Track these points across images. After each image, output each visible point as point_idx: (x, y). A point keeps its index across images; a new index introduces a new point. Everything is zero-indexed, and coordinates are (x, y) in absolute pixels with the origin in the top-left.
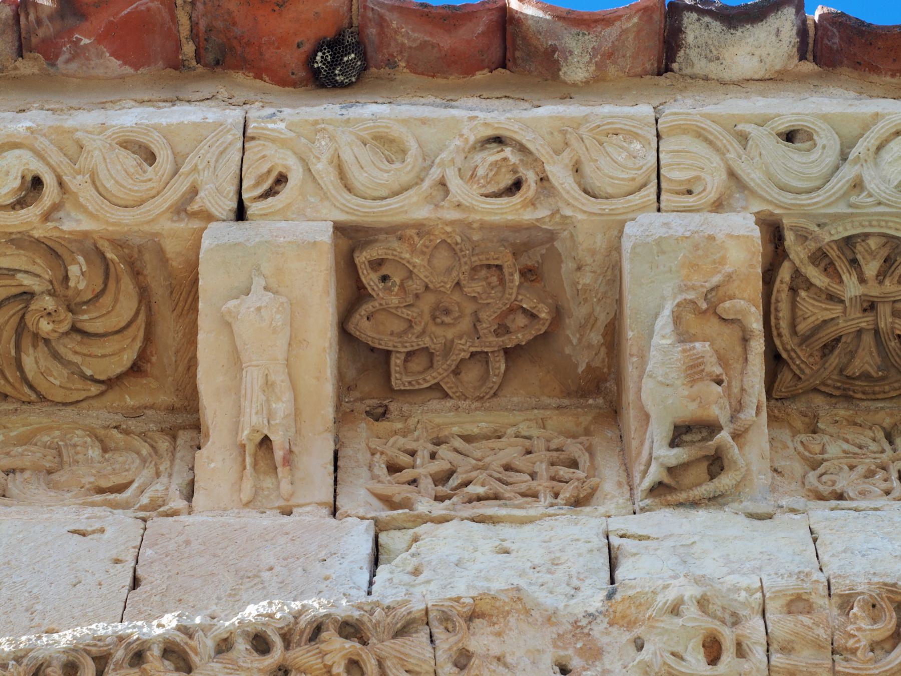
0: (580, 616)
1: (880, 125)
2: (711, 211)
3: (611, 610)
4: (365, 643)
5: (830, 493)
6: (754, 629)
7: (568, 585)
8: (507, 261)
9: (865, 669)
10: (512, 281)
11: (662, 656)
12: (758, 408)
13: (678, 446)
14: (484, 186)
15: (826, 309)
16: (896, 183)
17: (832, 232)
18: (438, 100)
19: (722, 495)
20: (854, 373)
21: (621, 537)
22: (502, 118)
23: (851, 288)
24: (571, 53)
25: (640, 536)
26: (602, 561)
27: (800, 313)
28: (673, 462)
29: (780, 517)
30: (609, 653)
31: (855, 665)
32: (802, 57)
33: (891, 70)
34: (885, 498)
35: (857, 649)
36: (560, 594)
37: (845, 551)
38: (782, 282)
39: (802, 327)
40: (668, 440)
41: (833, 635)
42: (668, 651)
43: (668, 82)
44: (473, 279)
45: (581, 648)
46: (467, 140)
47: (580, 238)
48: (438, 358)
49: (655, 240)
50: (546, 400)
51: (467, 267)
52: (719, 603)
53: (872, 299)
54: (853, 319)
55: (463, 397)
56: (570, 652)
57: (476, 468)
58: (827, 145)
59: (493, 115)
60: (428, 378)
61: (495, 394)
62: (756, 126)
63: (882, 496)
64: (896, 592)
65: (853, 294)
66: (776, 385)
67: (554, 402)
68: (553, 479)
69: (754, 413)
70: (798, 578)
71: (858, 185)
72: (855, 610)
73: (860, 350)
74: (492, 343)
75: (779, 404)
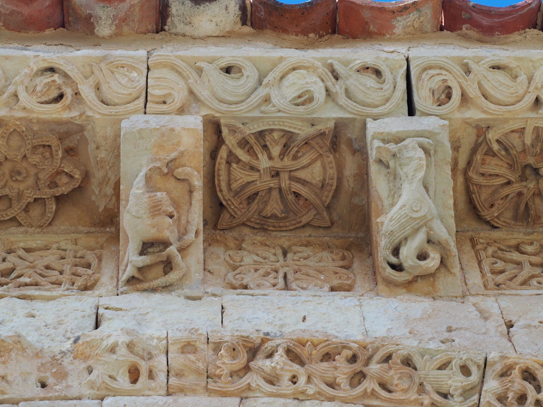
0: (57, 353)
1: (283, 64)
2: (176, 114)
3: (75, 350)
5: (240, 285)
6: (160, 362)
7: (64, 336)
8: (54, 142)
9: (226, 388)
10: (57, 155)
11: (102, 378)
12: (197, 233)
13: (145, 255)
14: (40, 97)
15: (249, 175)
16: (290, 99)
17: (251, 128)
18: (20, 46)
19: (171, 285)
20: (267, 215)
21: (106, 309)
22: (54, 57)
23: (264, 163)
24: (100, 18)
25: (116, 308)
26: (90, 322)
27: (232, 177)
28: (141, 265)
30: (71, 375)
31: (219, 385)
32: (244, 23)
33: (295, 32)
34: (272, 288)
35: (221, 375)
36: (58, 341)
37: (238, 319)
38: (221, 158)
39: (234, 186)
40: (139, 251)
41: (208, 367)
42: (107, 375)
43: (161, 37)
44: (34, 154)
45: (55, 372)
46: (32, 69)
47: (98, 129)
48: (15, 202)
49: (137, 131)
50: (81, 228)
51: (30, 146)
52: (141, 346)
53: (277, 169)
54: (265, 182)
55: (30, 226)
56: (48, 374)
57: (27, 267)
58: (250, 75)
59: (49, 54)
60: (9, 213)
61: (50, 224)
62: (207, 64)
63: (270, 287)
64: (248, 341)
65: (265, 166)
66: (220, 221)
67: (86, 229)
68: (74, 274)
69: (193, 235)
70: (190, 332)
71: (267, 100)
72: (222, 351)
73: (271, 200)
74: (47, 193)
75: (222, 232)
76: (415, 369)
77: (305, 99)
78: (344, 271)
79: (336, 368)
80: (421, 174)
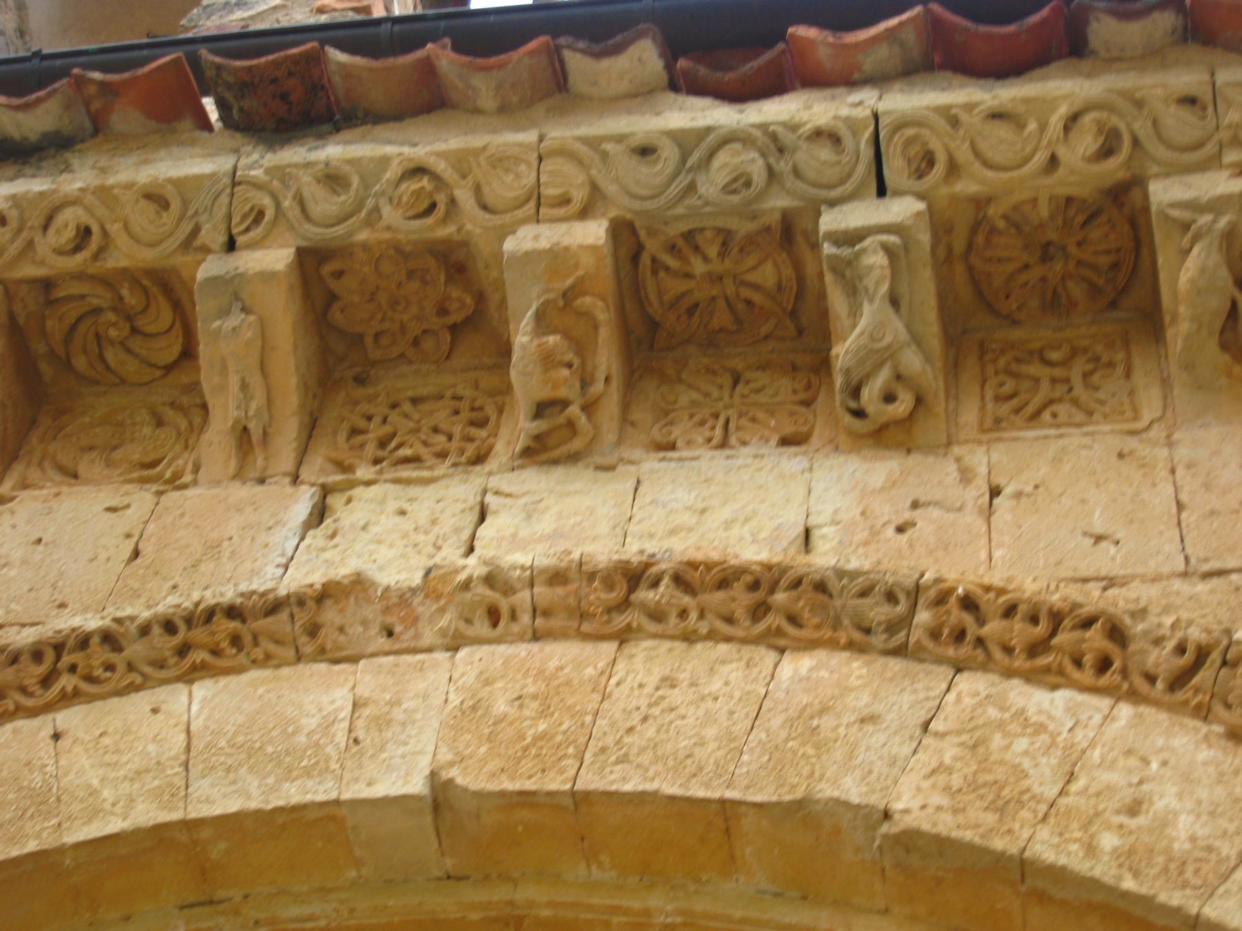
1: (712, 136)
4: (244, 621)
23: (699, 267)
28: (535, 432)
29: (621, 468)
39: (667, 298)
58: (670, 153)
61: (448, 357)
76: (831, 596)
77: (741, 181)
78: (802, 409)
79: (734, 600)
80: (884, 289)
